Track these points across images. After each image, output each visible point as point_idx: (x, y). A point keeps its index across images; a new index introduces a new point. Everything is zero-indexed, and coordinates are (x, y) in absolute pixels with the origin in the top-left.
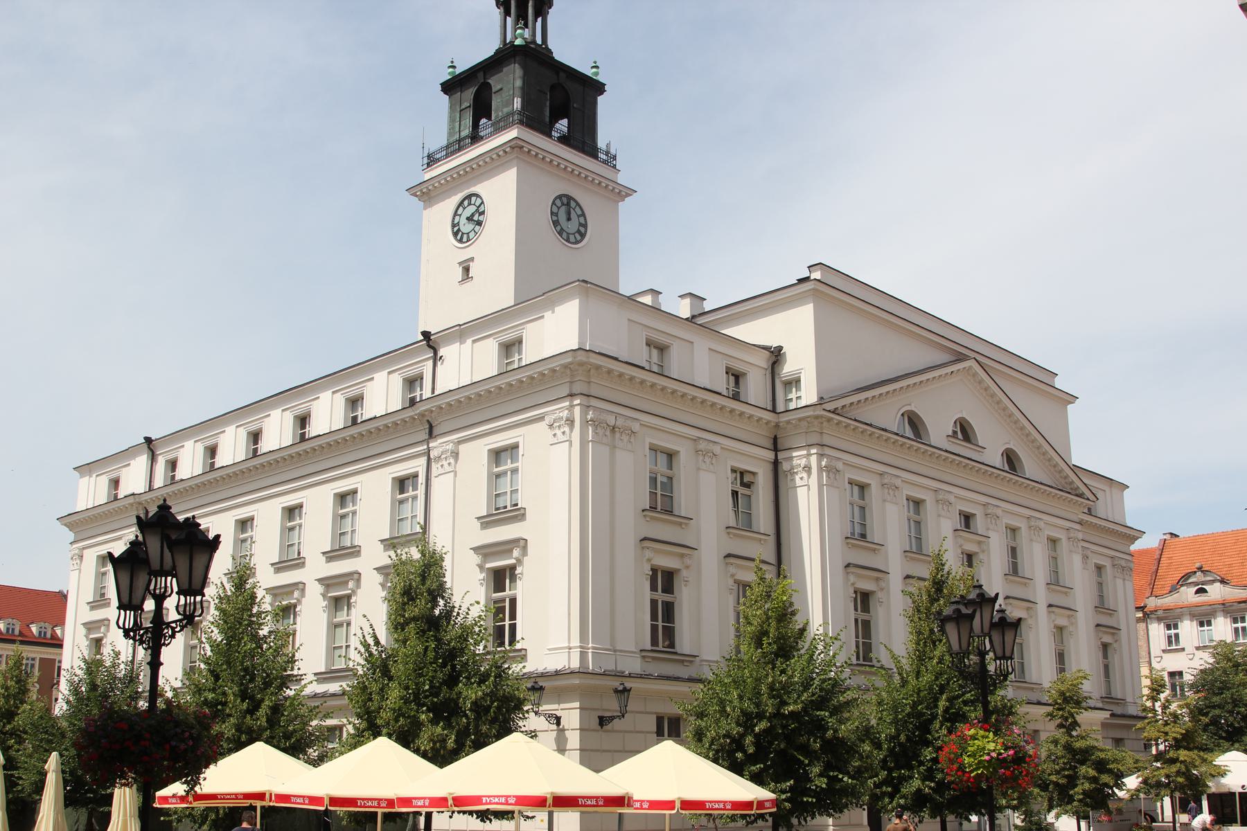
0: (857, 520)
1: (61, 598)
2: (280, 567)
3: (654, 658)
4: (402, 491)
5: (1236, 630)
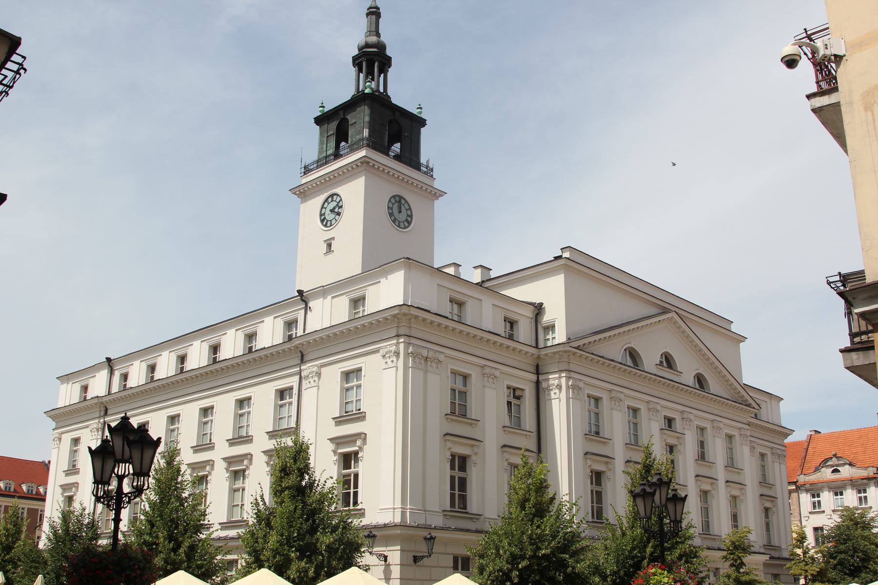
0: (593, 422)
1: (45, 467)
2: (197, 449)
3: (452, 516)
4: (282, 399)
5: (860, 498)
